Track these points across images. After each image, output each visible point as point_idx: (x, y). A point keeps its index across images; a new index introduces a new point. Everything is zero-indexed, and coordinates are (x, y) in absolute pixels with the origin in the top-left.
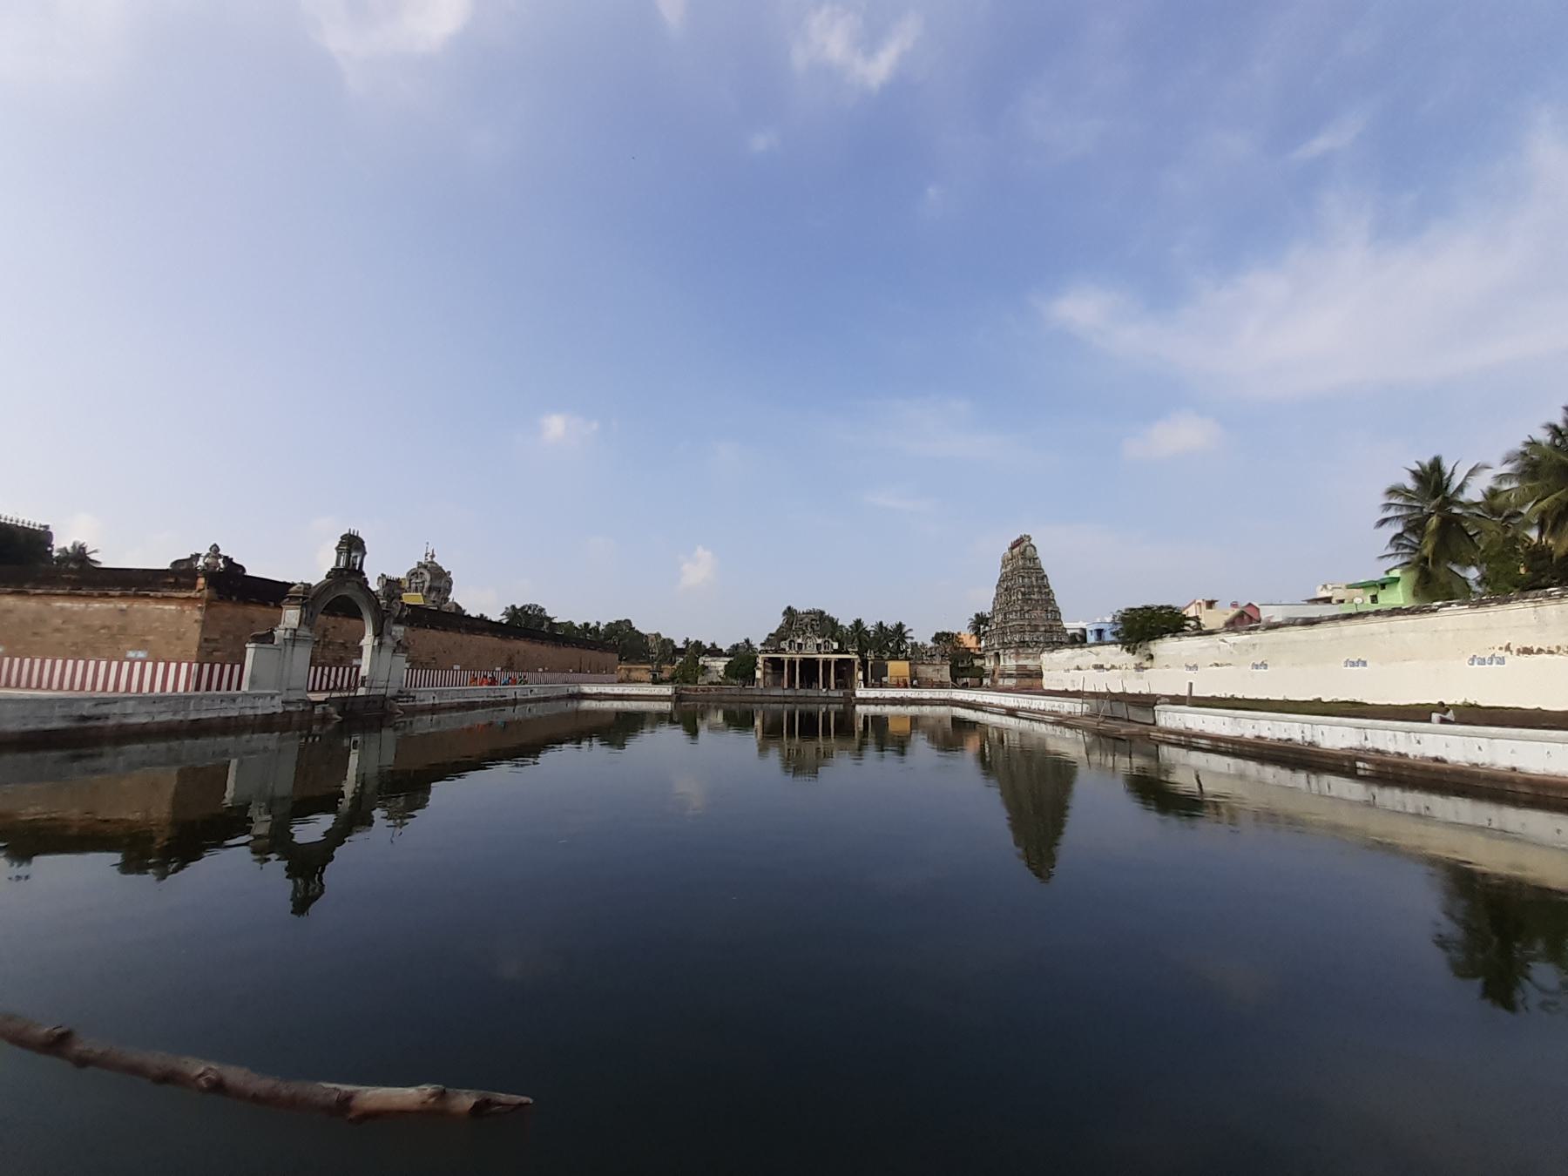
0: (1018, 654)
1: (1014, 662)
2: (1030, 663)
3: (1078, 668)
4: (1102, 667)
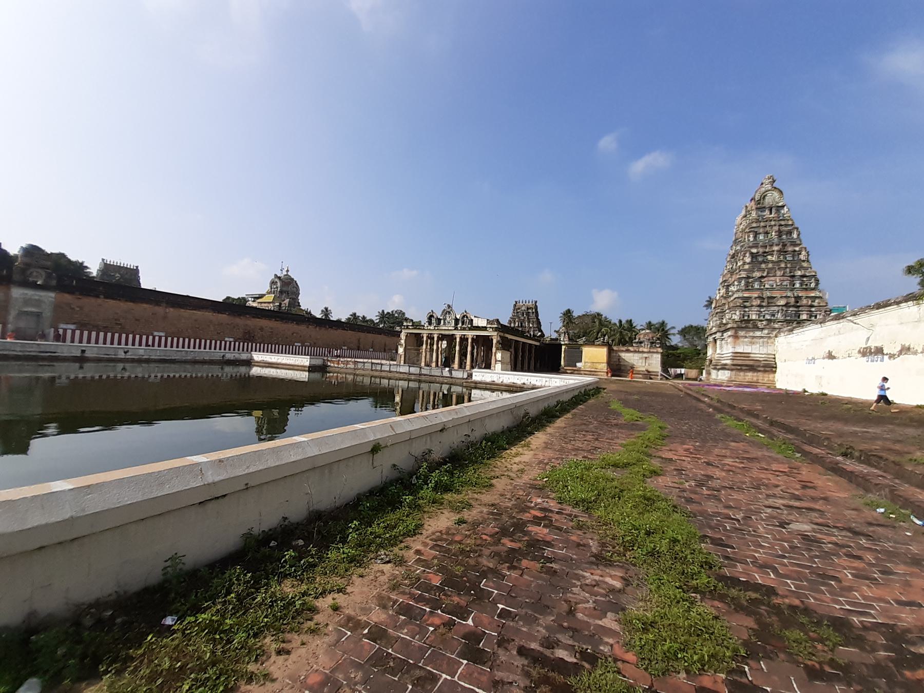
0: (736, 337)
1: (731, 350)
2: (756, 349)
3: (831, 356)
4: (879, 351)
